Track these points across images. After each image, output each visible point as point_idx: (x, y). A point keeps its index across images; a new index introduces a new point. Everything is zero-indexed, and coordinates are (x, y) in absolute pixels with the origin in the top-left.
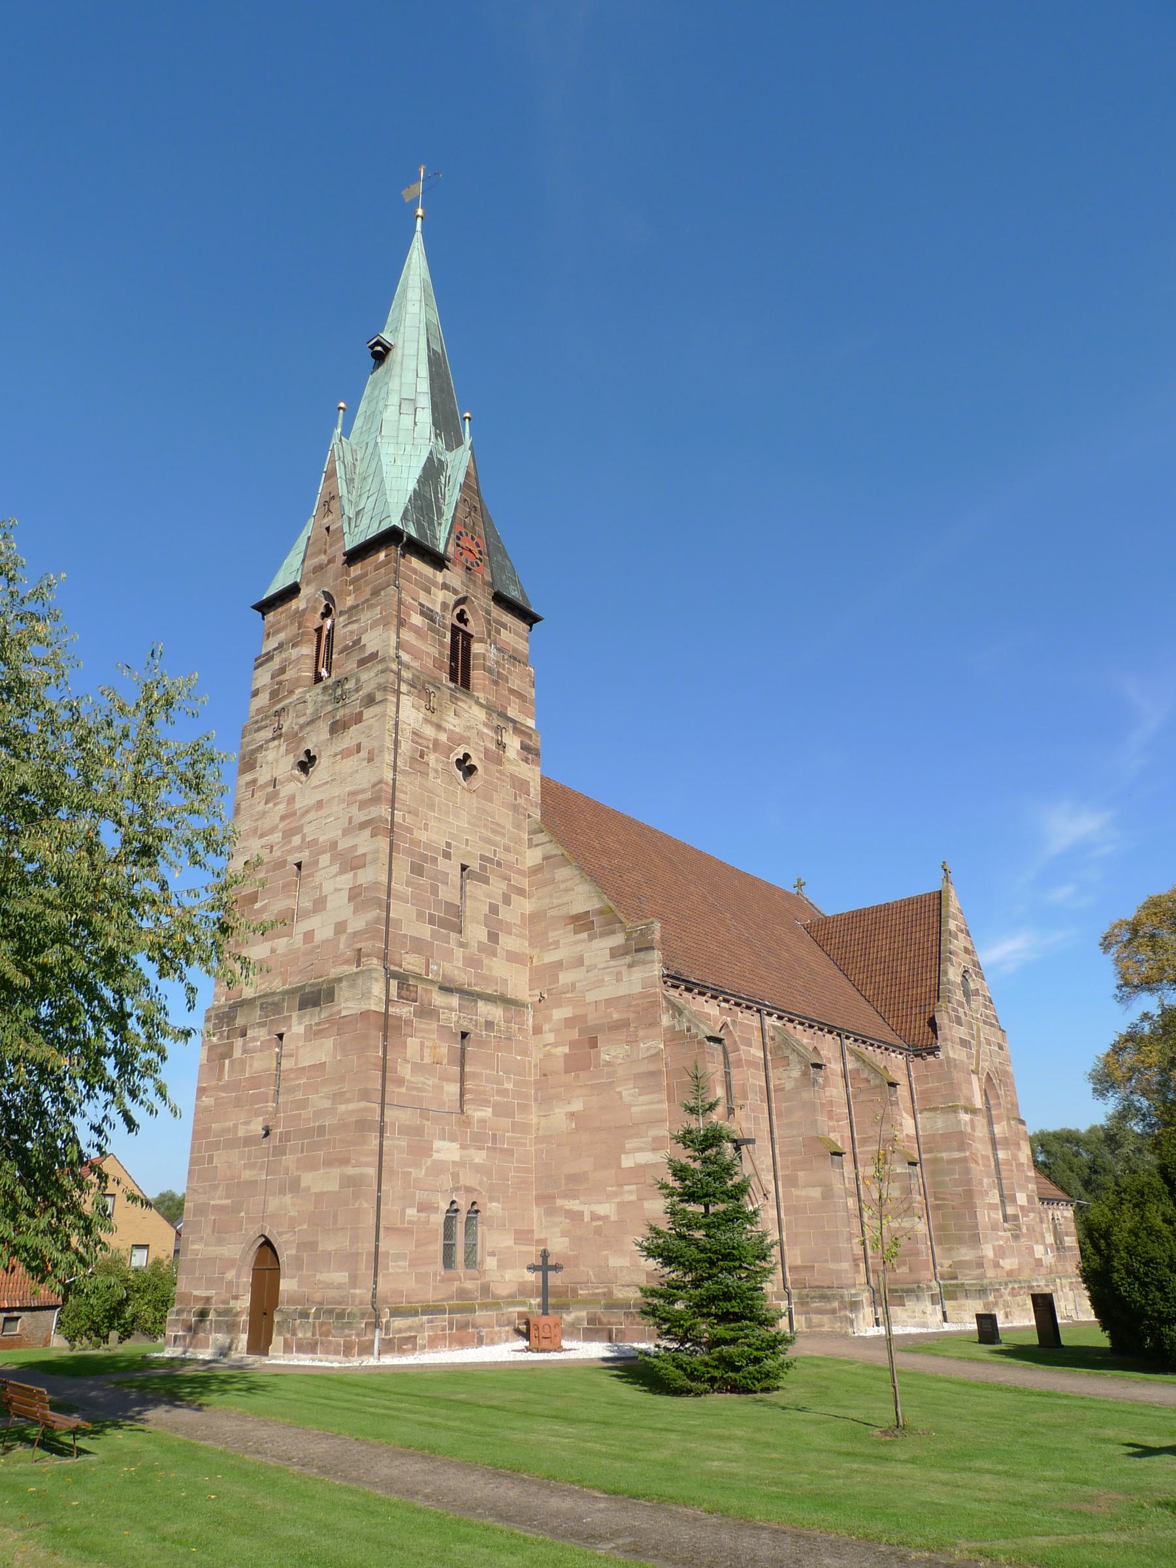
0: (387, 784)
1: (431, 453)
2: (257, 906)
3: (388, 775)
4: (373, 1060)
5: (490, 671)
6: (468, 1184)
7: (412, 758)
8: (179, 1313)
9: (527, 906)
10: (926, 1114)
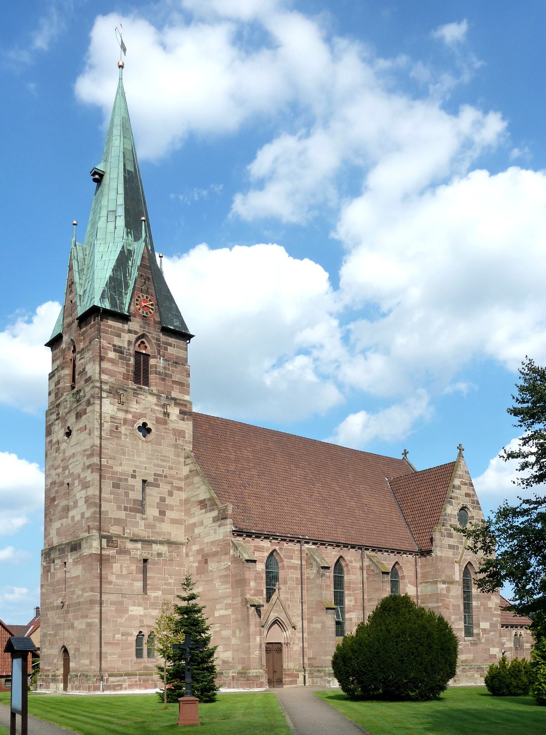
0: (97, 446)
1: (123, 246)
2: (56, 503)
3: (97, 442)
4: (95, 575)
5: (159, 373)
6: (148, 624)
7: (111, 431)
8: (41, 676)
9: (183, 495)
10: (423, 585)
